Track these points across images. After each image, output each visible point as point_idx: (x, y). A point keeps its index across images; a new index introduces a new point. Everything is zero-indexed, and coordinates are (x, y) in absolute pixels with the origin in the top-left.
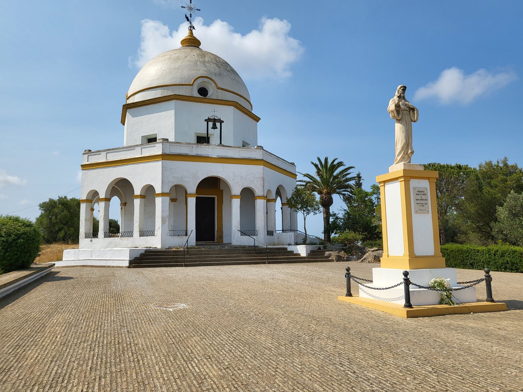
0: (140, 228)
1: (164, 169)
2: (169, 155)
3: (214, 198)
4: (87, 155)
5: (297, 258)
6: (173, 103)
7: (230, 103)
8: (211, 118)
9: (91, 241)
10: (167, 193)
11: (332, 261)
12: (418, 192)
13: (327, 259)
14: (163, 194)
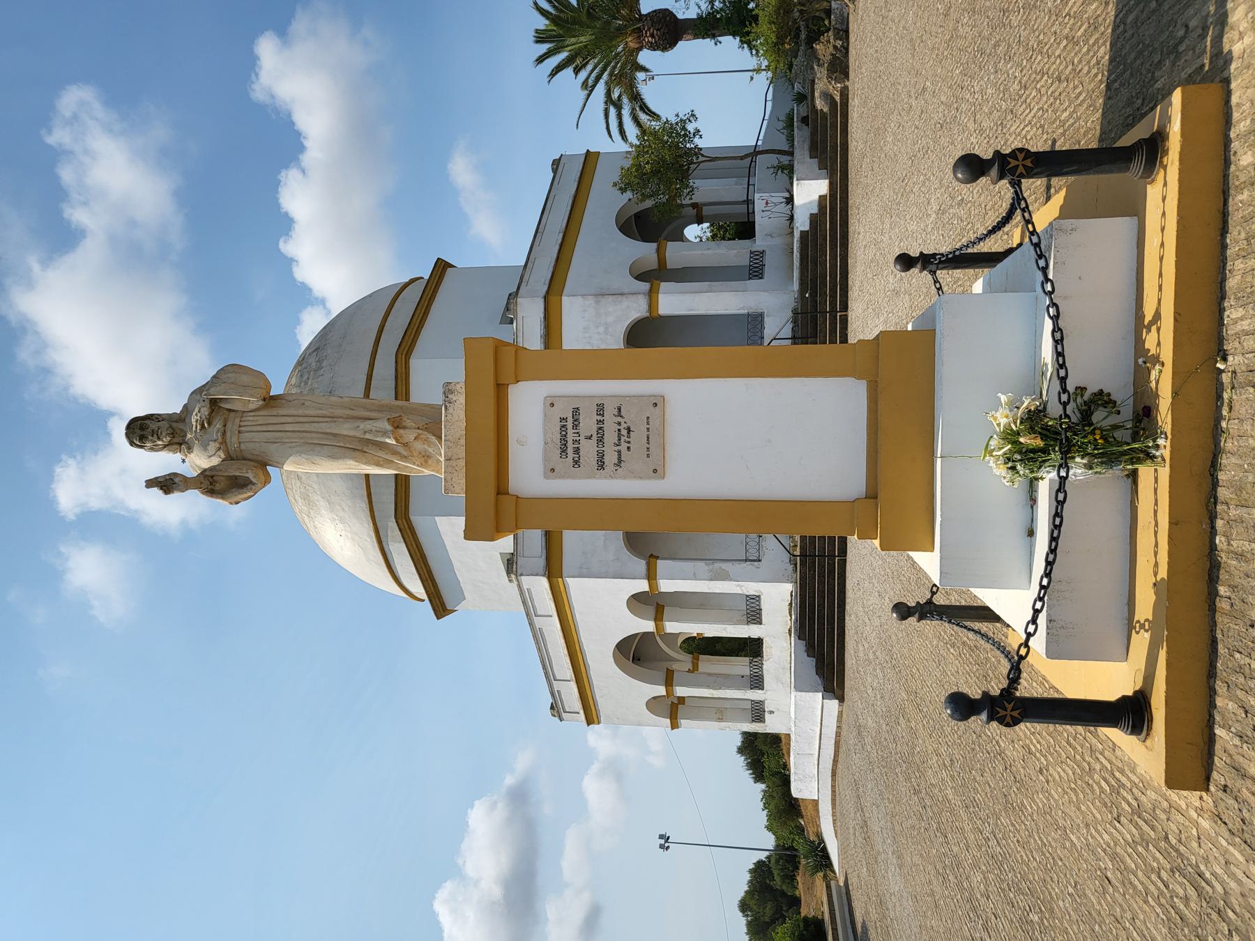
0: (739, 623)
1: (585, 572)
2: (548, 559)
4: (564, 715)
5: (833, 209)
6: (417, 520)
7: (402, 370)
9: (771, 712)
10: (648, 564)
11: (845, 93)
12: (564, 451)
13: (840, 108)
14: (651, 576)
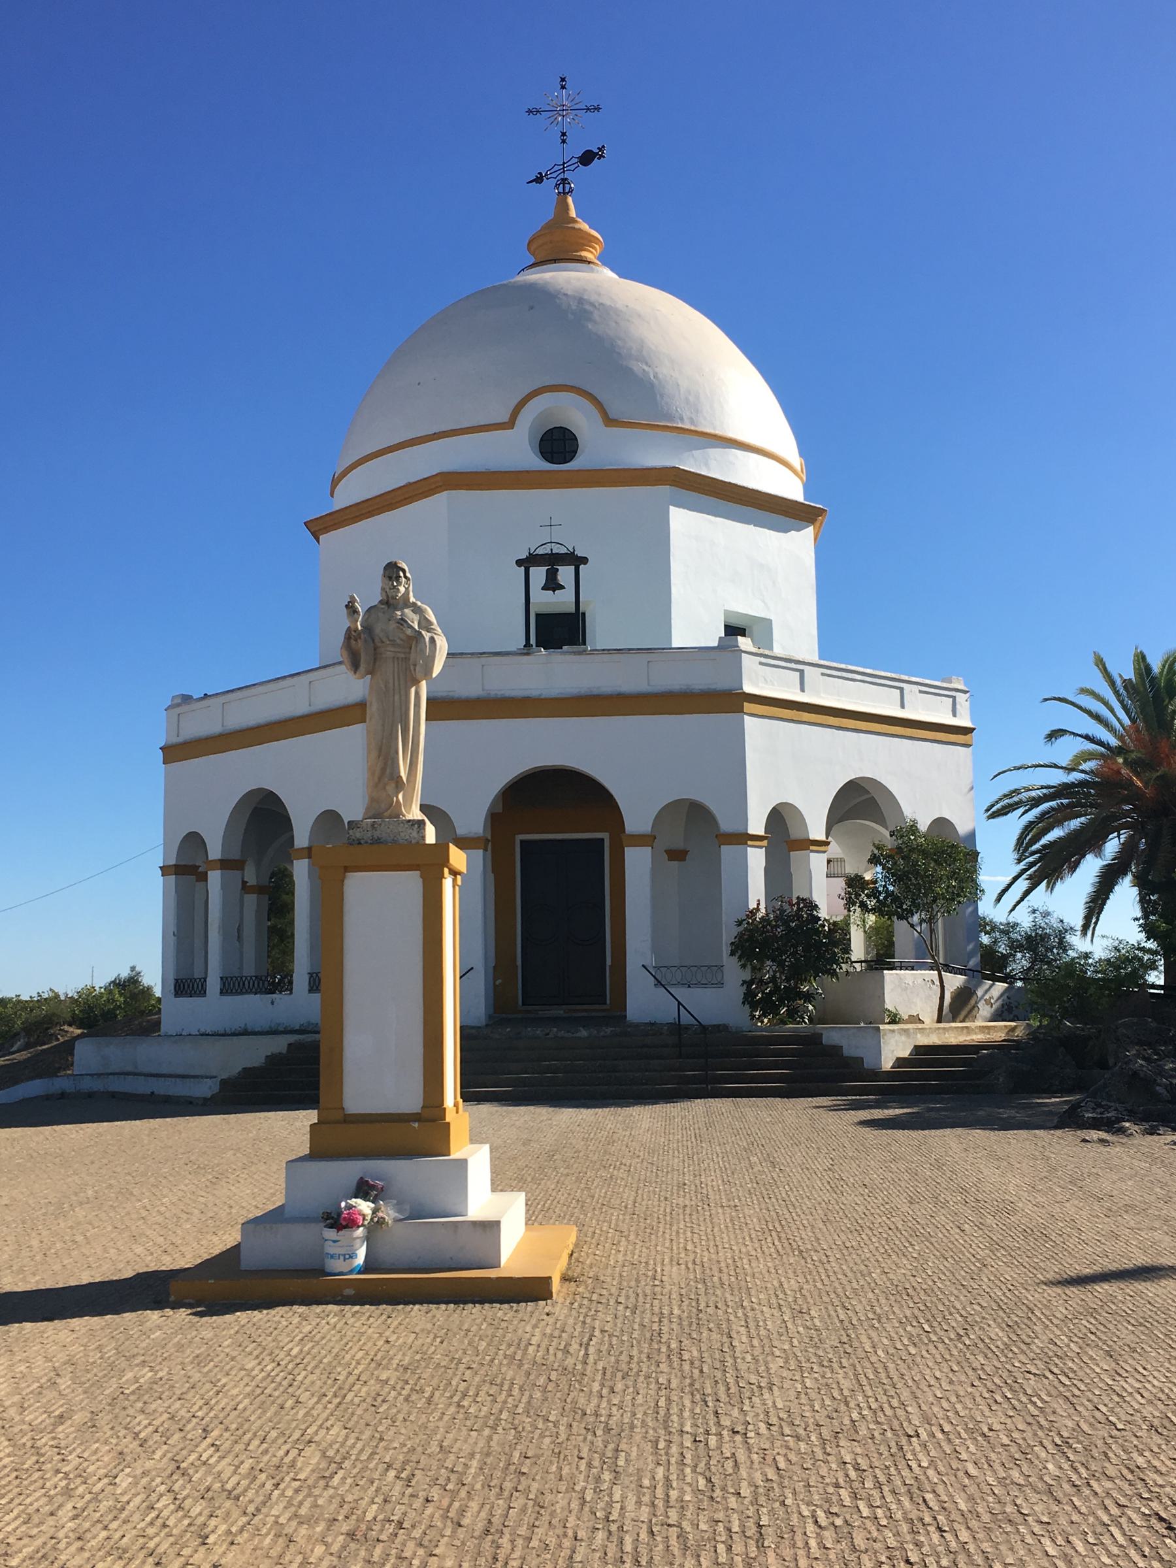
3: (603, 840)
8: (540, 551)
